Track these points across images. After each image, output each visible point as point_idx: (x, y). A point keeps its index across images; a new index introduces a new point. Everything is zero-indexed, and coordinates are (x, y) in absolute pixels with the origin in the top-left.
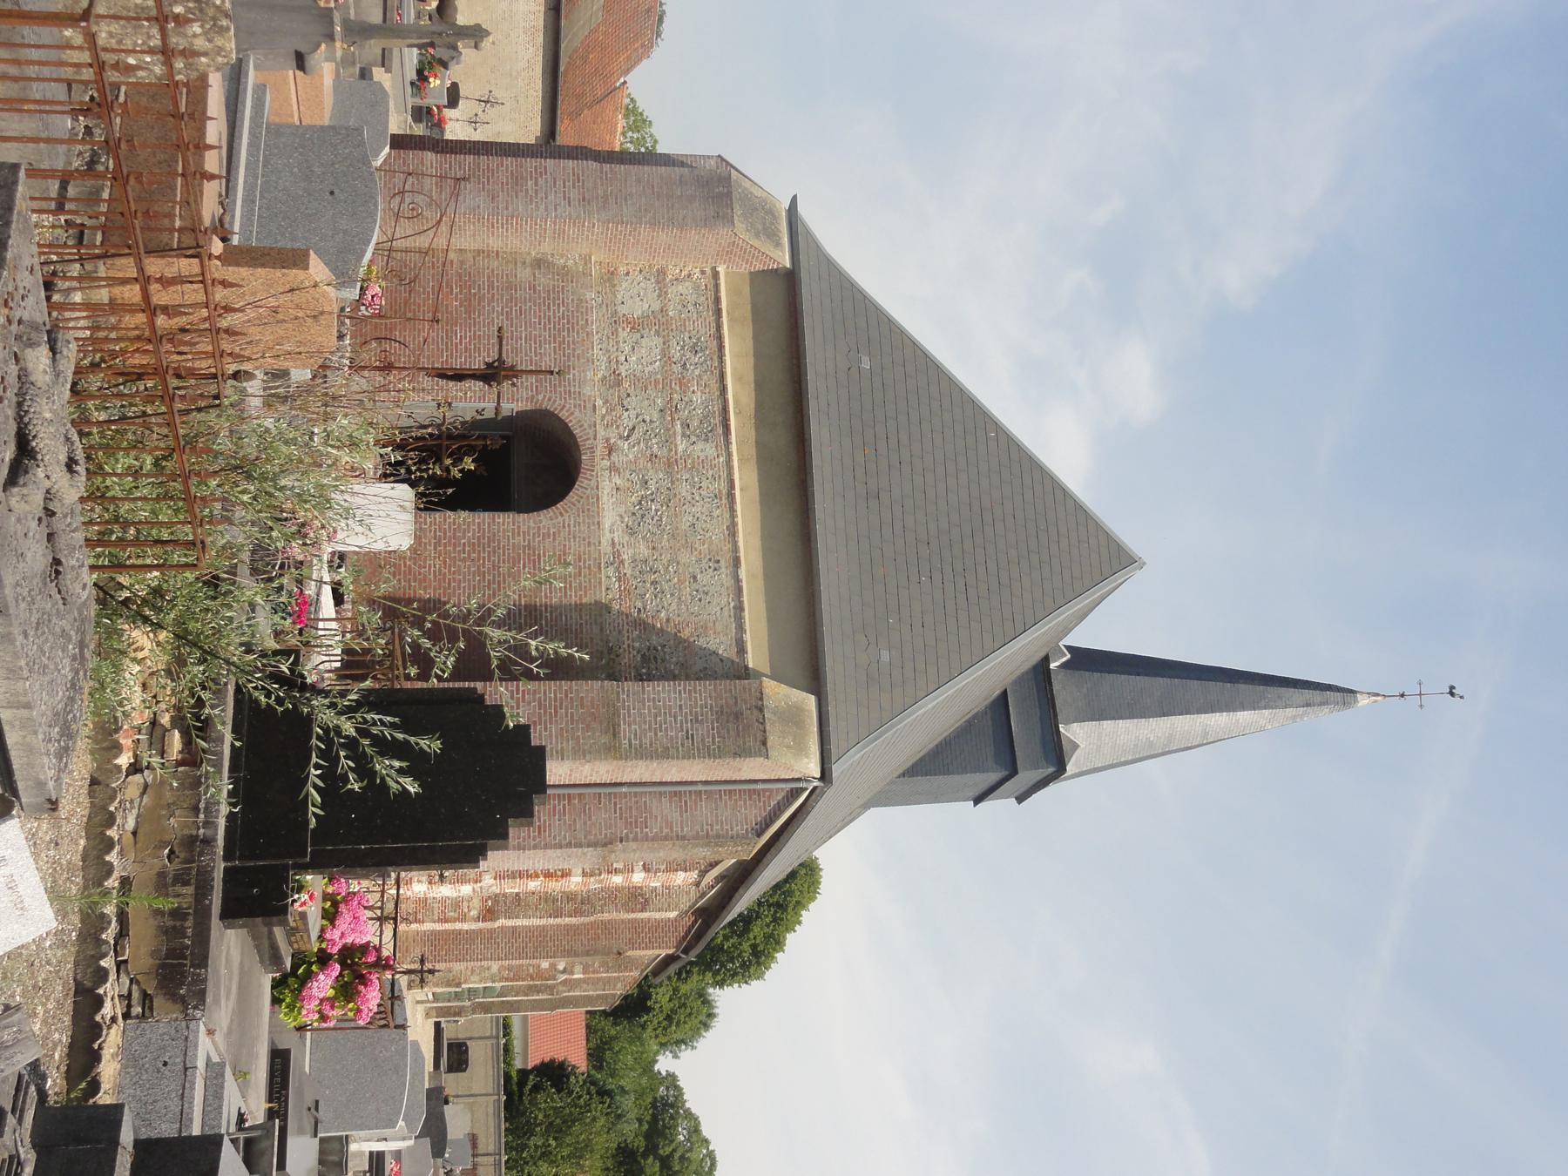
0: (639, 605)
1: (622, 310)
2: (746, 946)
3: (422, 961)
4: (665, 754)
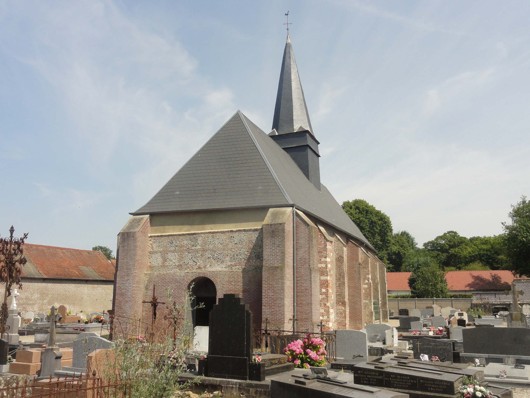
0: (243, 260)
1: (160, 264)
2: (380, 222)
3: (318, 326)
4: (283, 253)
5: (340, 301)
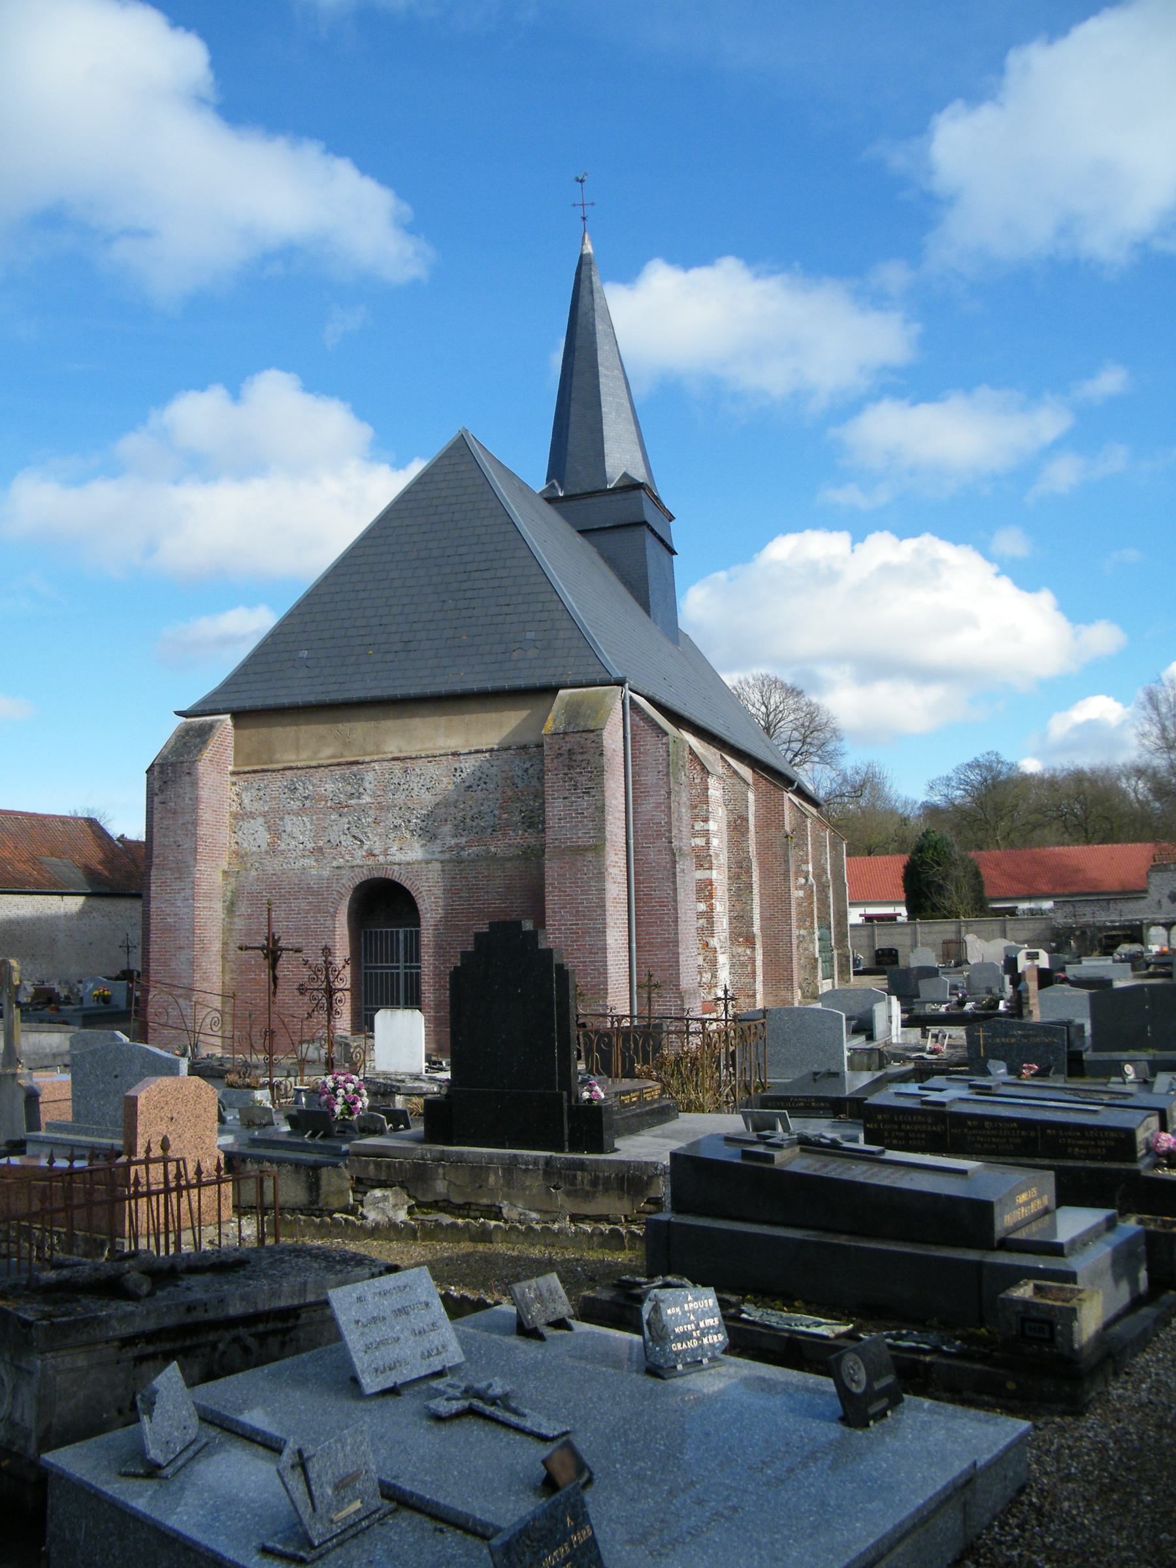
1: (264, 847)
4: (601, 809)
5: (742, 935)
